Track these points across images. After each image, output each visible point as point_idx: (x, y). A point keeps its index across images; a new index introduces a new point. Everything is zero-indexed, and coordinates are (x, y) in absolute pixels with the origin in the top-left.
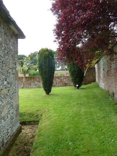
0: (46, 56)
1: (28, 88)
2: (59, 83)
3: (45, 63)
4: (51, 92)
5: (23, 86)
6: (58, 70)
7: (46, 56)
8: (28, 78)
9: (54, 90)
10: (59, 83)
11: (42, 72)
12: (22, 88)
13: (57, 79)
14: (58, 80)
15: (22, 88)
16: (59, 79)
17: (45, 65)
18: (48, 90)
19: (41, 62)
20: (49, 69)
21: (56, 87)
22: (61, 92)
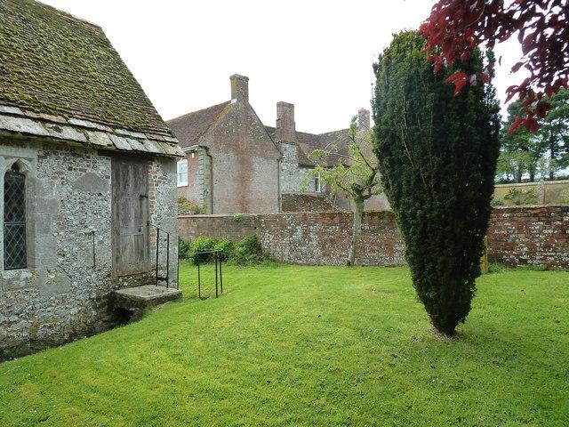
0: (417, 72)
1: (380, 265)
2: (547, 247)
3: (411, 120)
4: (472, 314)
5: (353, 258)
6: (560, 179)
7: (417, 72)
8: (380, 218)
9: (498, 294)
10: (547, 247)
11: (400, 186)
12: (349, 264)
13: (536, 226)
14: (540, 232)
15: (349, 264)
16: (549, 223)
17: (411, 134)
18: (447, 300)
19: (386, 115)
20: (447, 161)
21: (531, 268)
22: (550, 324)
